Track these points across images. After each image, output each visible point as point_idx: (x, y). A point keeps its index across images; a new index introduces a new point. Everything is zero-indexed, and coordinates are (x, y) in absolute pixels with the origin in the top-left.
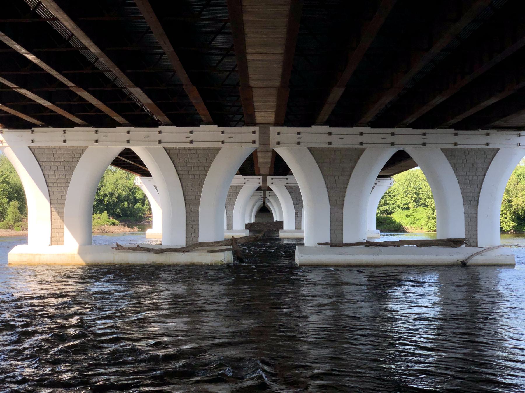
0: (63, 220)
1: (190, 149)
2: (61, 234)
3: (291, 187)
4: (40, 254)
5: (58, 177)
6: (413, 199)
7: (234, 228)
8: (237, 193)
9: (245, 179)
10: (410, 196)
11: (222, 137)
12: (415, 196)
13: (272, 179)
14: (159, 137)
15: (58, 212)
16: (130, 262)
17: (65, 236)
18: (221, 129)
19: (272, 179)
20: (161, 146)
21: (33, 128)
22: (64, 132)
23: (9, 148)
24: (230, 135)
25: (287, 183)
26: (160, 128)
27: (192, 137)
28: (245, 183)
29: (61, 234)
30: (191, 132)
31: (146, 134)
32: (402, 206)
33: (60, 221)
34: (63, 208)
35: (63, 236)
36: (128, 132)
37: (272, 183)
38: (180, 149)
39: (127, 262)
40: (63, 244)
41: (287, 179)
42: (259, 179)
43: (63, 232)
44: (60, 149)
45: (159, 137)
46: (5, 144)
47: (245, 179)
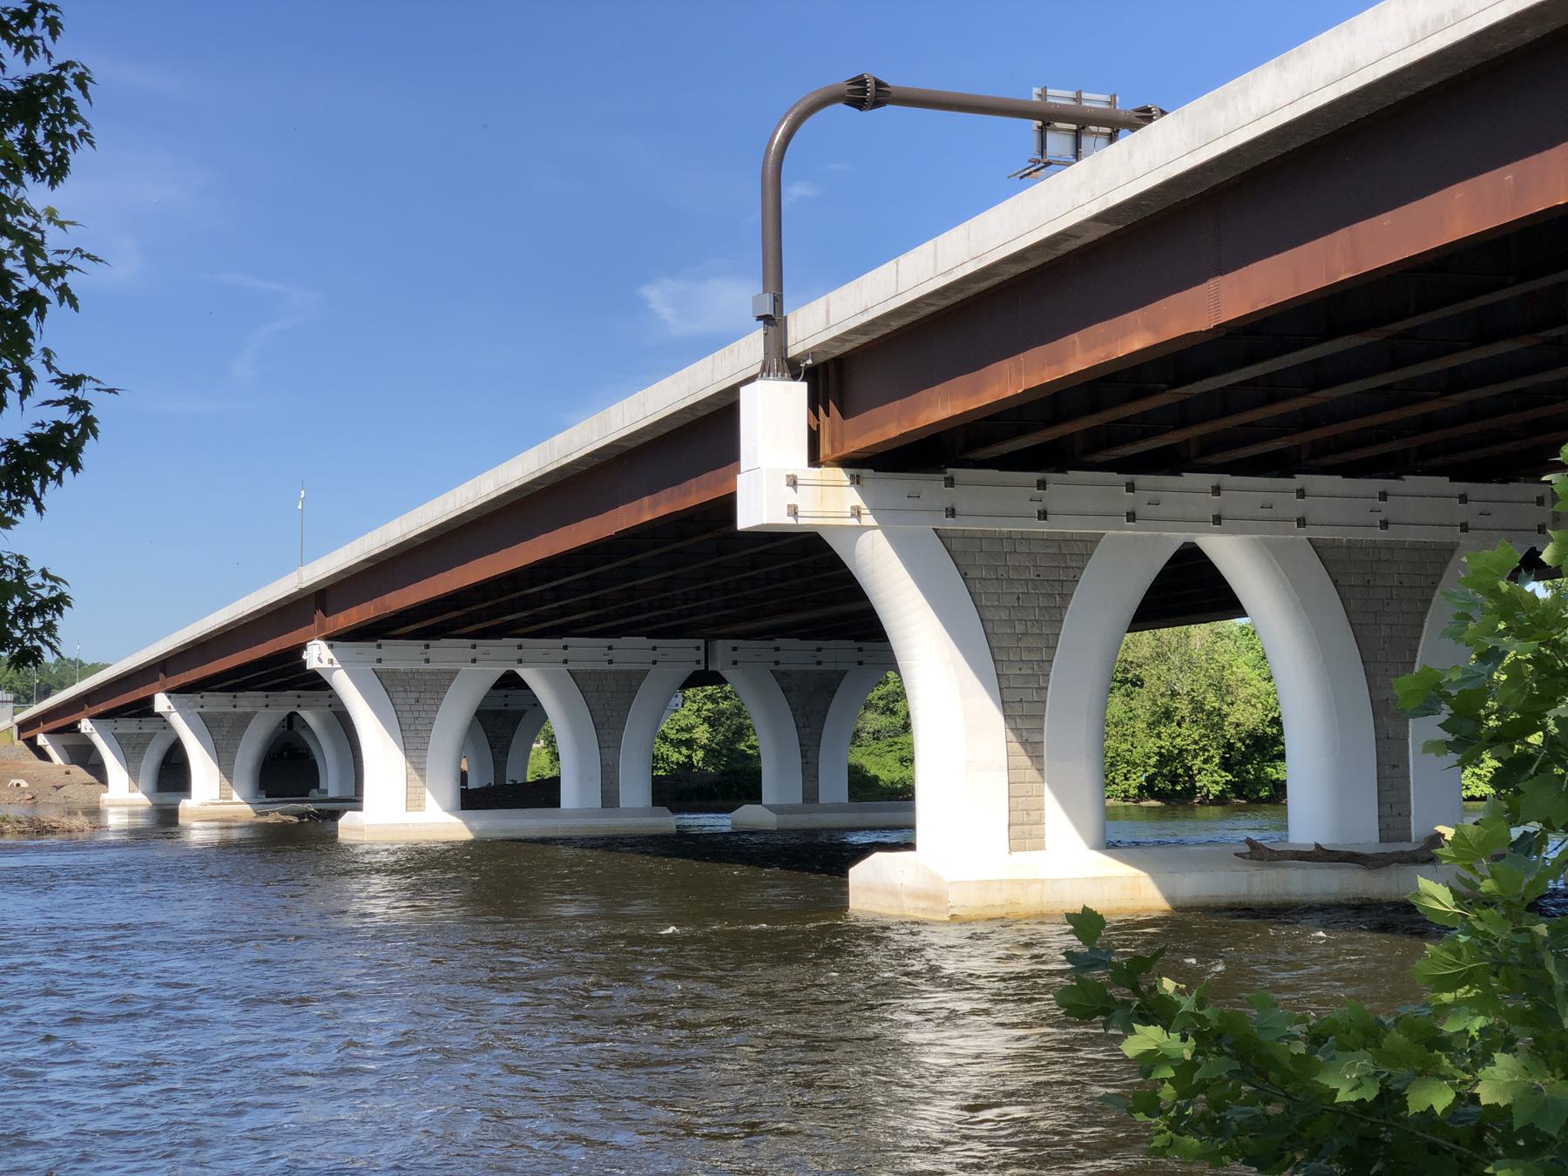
0: (1041, 770)
1: (1374, 546)
2: (1034, 816)
3: (786, 674)
4: (1042, 881)
5: (1020, 628)
6: (704, 713)
7: (825, 797)
8: (632, 693)
9: (654, 648)
10: (695, 707)
11: (1462, 513)
12: (709, 706)
13: (735, 649)
14: (1298, 507)
15: (1024, 743)
16: (1293, 898)
17: (1047, 820)
18: (1460, 487)
19: (735, 649)
20: (1302, 535)
21: (950, 471)
22: (1042, 485)
23: (879, 534)
24: (1483, 506)
25: (777, 663)
26: (1300, 480)
27: (1388, 509)
28: (654, 662)
29: (1034, 816)
30: (1383, 496)
31: (1261, 497)
32: (672, 735)
33: (1032, 773)
34: (1041, 730)
35: (1040, 822)
36: (1217, 490)
37: (735, 663)
38: (1351, 546)
39: (1286, 898)
40: (1041, 847)
41: (777, 649)
42: (698, 648)
43: (1041, 809)
44: (1025, 538)
45: (1298, 507)
46: (869, 520)
47: (654, 648)
